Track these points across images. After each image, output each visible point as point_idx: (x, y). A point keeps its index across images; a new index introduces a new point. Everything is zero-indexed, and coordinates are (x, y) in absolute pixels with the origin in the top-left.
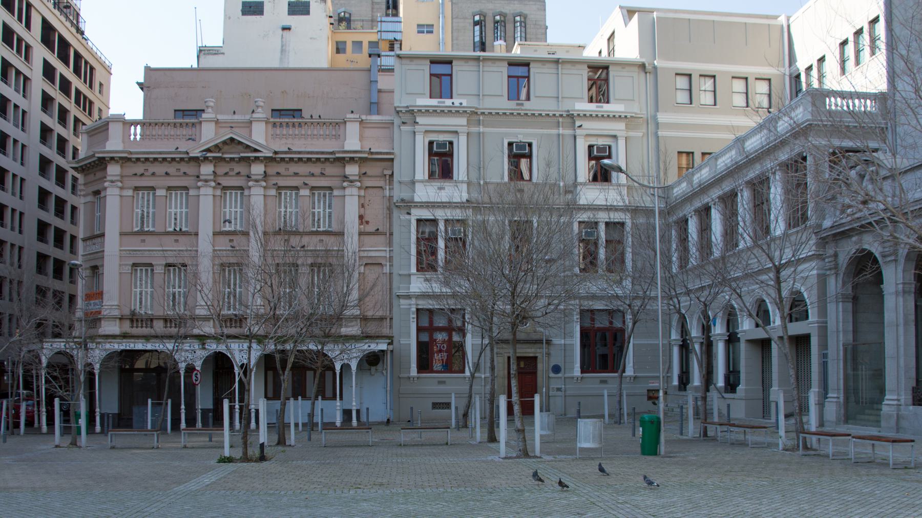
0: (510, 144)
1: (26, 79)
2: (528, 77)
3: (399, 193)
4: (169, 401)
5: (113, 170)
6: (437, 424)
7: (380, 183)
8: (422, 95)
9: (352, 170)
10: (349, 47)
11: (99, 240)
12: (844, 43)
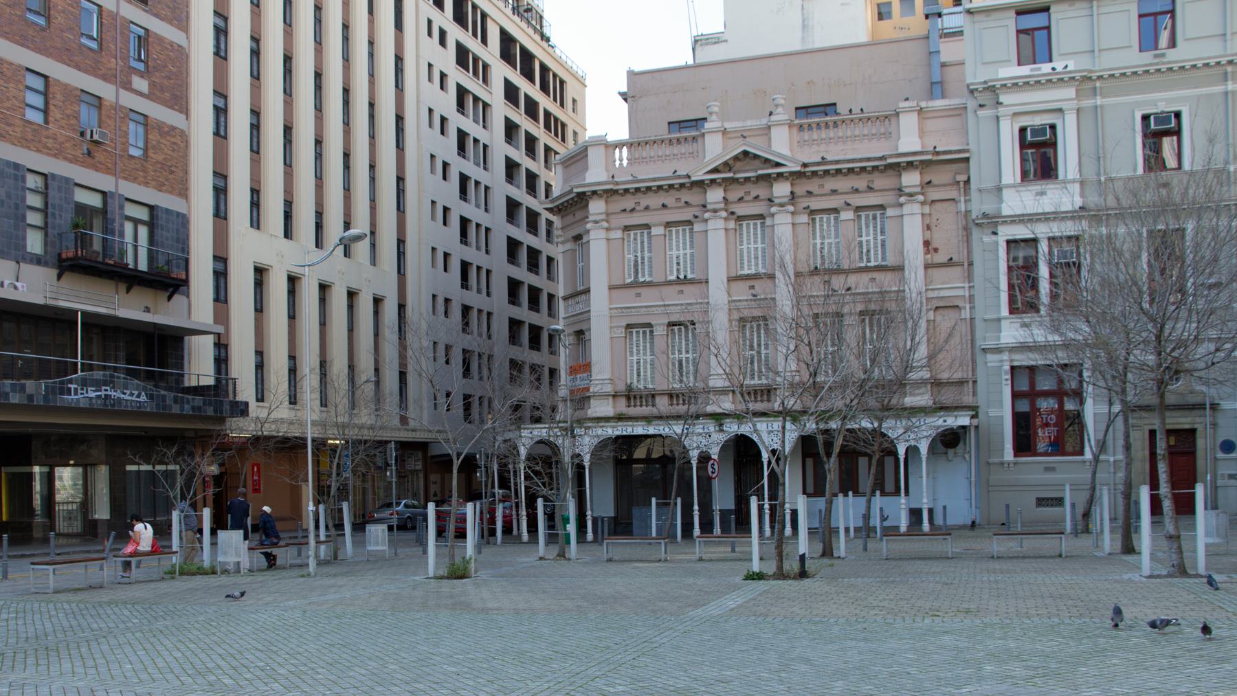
0: (1145, 118)
3: (979, 205)
5: (596, 207)
7: (952, 194)
9: (911, 179)
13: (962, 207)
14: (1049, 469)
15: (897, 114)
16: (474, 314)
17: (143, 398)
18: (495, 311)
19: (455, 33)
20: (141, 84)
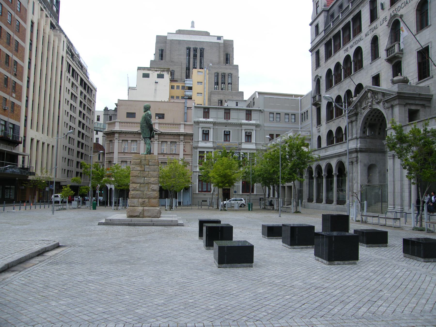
0: (224, 131)
1: (76, 97)
2: (227, 141)
3: (195, 145)
4: (30, 196)
5: (117, 135)
6: (8, 260)
7: (189, 141)
8: (201, 117)
9: (182, 137)
10: (175, 87)
11: (112, 154)
13: (191, 144)
14: (205, 195)
15: (180, 124)
16: (84, 155)
17: (19, 171)
18: (75, 149)
19: (72, 79)
20: (14, 95)
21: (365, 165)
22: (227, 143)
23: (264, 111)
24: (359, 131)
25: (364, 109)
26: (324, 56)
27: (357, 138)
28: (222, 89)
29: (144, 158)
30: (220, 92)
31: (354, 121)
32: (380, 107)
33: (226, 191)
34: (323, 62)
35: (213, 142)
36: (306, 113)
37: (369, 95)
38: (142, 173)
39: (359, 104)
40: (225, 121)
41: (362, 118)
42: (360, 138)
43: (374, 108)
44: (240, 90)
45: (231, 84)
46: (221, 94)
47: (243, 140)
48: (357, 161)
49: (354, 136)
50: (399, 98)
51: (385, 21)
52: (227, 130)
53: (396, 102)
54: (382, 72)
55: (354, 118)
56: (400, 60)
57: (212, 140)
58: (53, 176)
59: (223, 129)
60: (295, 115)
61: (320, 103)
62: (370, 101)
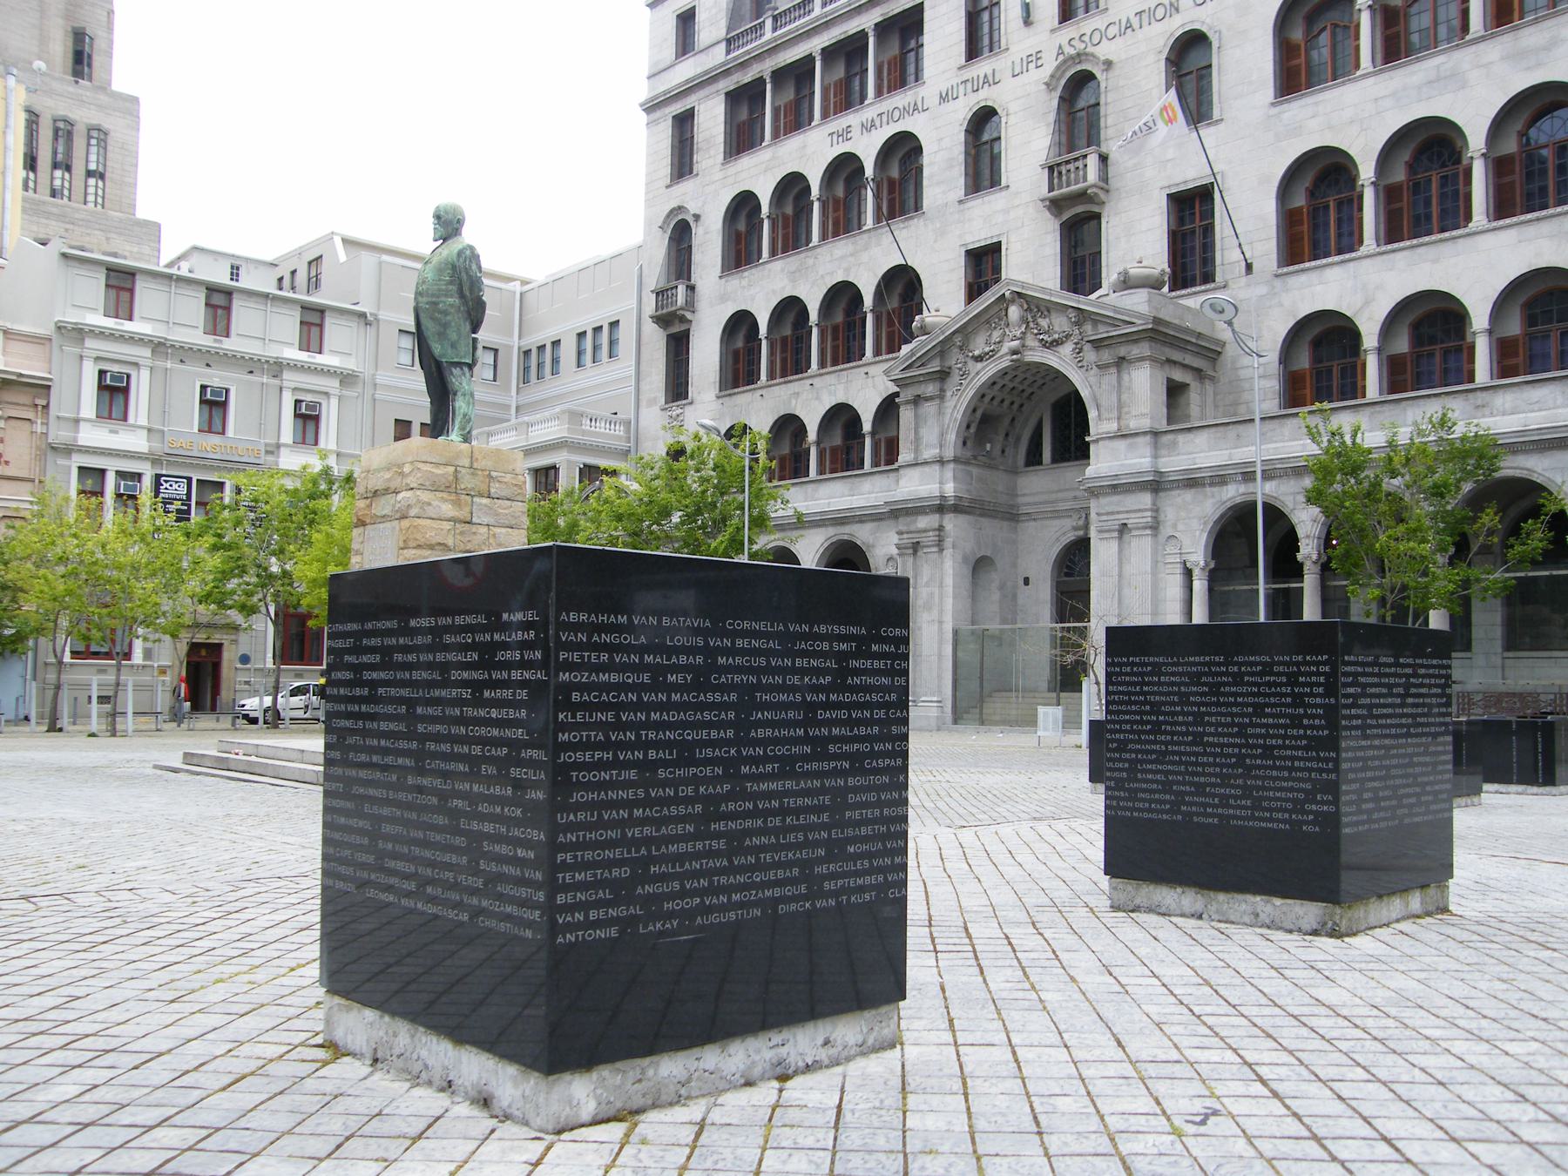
0: (204, 388)
3: (59, 434)
12: (582, 335)
13: (39, 428)
21: (965, 559)
22: (215, 440)
23: (377, 320)
24: (952, 437)
25: (979, 359)
26: (721, 138)
27: (941, 462)
28: (54, 193)
29: (466, 462)
30: (44, 203)
31: (927, 399)
32: (1061, 360)
33: (203, 653)
34: (711, 162)
35: (149, 430)
36: (549, 348)
37: (1014, 312)
38: (462, 533)
39: (958, 340)
40: (208, 341)
41: (969, 393)
42: (956, 460)
43: (1028, 359)
44: (142, 213)
45: (102, 176)
46: (48, 215)
47: (287, 435)
48: (940, 544)
49: (929, 453)
50: (1152, 339)
51: (1032, 66)
52: (216, 382)
53: (1144, 349)
54: (1013, 238)
55: (930, 389)
56: (1096, 209)
57: (143, 421)
58: (520, 508)
59: (196, 377)
60: (496, 351)
61: (689, 316)
62: (1018, 334)
